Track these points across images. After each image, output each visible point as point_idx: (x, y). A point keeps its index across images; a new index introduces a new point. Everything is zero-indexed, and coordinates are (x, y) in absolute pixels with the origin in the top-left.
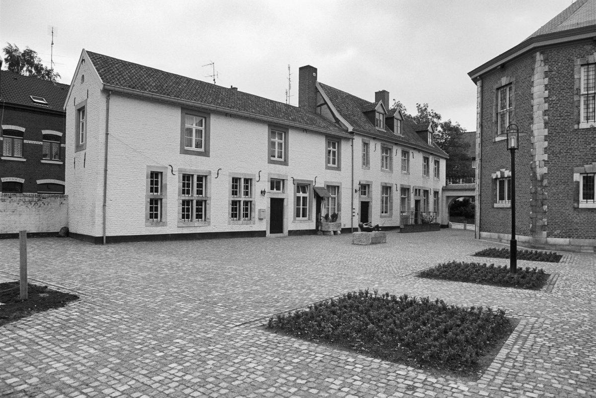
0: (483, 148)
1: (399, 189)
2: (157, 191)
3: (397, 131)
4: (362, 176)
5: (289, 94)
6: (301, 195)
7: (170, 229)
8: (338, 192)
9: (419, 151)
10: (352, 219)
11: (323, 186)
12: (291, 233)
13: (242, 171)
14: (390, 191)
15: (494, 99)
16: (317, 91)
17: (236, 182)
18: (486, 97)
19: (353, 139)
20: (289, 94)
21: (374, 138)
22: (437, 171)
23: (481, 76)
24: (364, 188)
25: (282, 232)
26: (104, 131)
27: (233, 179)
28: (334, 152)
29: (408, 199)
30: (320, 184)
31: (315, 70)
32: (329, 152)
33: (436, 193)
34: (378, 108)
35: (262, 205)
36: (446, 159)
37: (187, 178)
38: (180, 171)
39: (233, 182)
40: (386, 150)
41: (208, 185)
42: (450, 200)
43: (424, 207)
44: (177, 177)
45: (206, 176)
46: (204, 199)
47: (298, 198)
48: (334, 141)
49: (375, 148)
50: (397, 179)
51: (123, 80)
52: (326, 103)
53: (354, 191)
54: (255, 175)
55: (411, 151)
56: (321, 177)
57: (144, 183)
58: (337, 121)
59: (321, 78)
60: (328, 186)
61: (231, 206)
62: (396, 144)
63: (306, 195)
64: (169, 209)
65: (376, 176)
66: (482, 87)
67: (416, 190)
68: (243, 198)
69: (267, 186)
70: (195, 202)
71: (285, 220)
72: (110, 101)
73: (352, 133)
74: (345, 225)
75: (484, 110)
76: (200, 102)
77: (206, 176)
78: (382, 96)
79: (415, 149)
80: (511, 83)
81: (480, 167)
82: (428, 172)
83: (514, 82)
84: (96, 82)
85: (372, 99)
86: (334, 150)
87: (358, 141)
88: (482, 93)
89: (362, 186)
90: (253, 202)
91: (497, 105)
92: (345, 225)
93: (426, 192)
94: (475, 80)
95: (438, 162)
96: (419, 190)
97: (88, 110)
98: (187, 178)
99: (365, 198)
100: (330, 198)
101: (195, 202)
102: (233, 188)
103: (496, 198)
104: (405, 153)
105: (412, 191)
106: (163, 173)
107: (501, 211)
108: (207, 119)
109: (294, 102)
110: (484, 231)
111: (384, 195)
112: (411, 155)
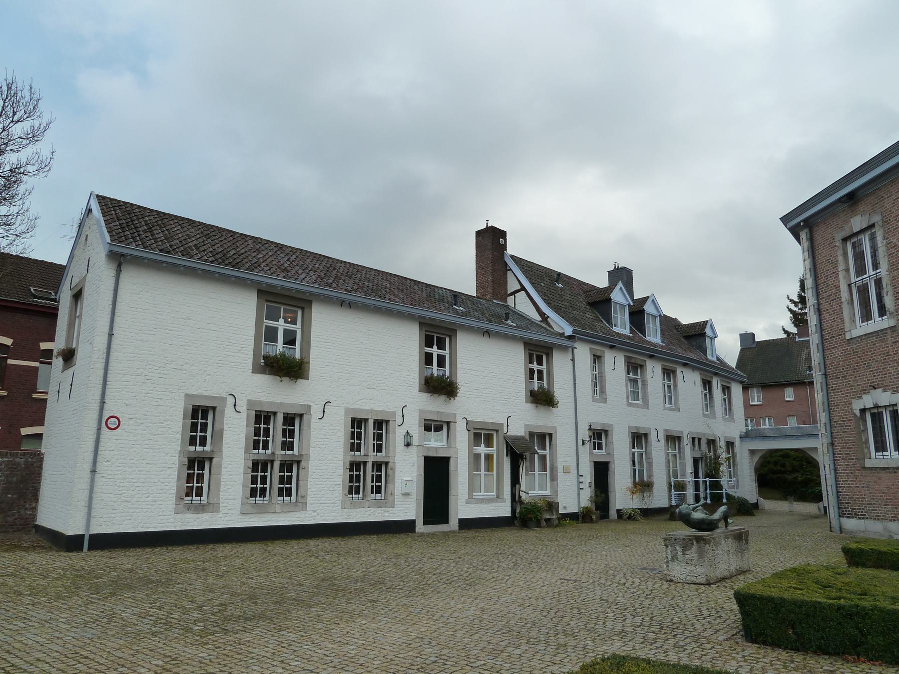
0: (827, 352)
1: (662, 437)
2: (203, 443)
3: (654, 336)
4: (594, 414)
5: (455, 268)
6: (482, 449)
7: (227, 518)
8: (550, 444)
9: (694, 368)
10: (579, 494)
11: (523, 434)
12: (465, 524)
13: (372, 404)
14: (646, 442)
15: (840, 258)
16: (505, 268)
17: (360, 427)
18: (820, 259)
19: (573, 349)
20: (455, 268)
21: (612, 347)
22: (728, 402)
23: (805, 223)
24: (598, 436)
25: (445, 520)
26: (106, 329)
27: (353, 420)
28: (540, 373)
29: (680, 457)
30: (517, 429)
31: (503, 234)
32: (532, 371)
33: (730, 445)
34: (618, 296)
35: (407, 473)
36: (742, 382)
37: (262, 418)
38: (250, 403)
39: (353, 427)
40: (634, 367)
41: (304, 431)
42: (756, 458)
43: (730, 472)
44: (244, 415)
45: (301, 416)
46: (296, 459)
47: (477, 457)
48: (539, 352)
49: (615, 365)
50: (657, 419)
51: (139, 235)
52: (523, 288)
53: (580, 443)
54: (394, 413)
55: (679, 370)
56: (521, 419)
57: (176, 425)
58: (544, 317)
59: (513, 249)
60: (532, 434)
61: (348, 473)
62: (651, 357)
63: (492, 450)
64: (224, 478)
65: (619, 414)
66: (811, 240)
67: (693, 439)
68: (373, 457)
69: (416, 430)
70: (277, 465)
71: (452, 499)
72: (121, 276)
73: (570, 338)
74: (565, 508)
75: (820, 282)
76: (289, 284)
77: (301, 416)
78: (621, 275)
79: (685, 365)
80: (872, 226)
81: (824, 388)
82: (712, 406)
83: (880, 223)
84: (100, 240)
85: (601, 281)
86: (540, 367)
87: (583, 352)
88: (812, 252)
89: (594, 433)
90: (390, 465)
91: (847, 270)
92: (565, 508)
93: (711, 442)
94: (795, 232)
95: (729, 388)
96: (699, 439)
97: (86, 293)
98: (262, 418)
99: (601, 455)
100: (536, 456)
101: (369, 467)
102: (352, 438)
103: (868, 448)
104: (668, 373)
105: (686, 441)
106: (217, 409)
107: (885, 475)
108: (306, 310)
109: (469, 287)
110: (850, 516)
111: (636, 449)
112: (679, 376)
